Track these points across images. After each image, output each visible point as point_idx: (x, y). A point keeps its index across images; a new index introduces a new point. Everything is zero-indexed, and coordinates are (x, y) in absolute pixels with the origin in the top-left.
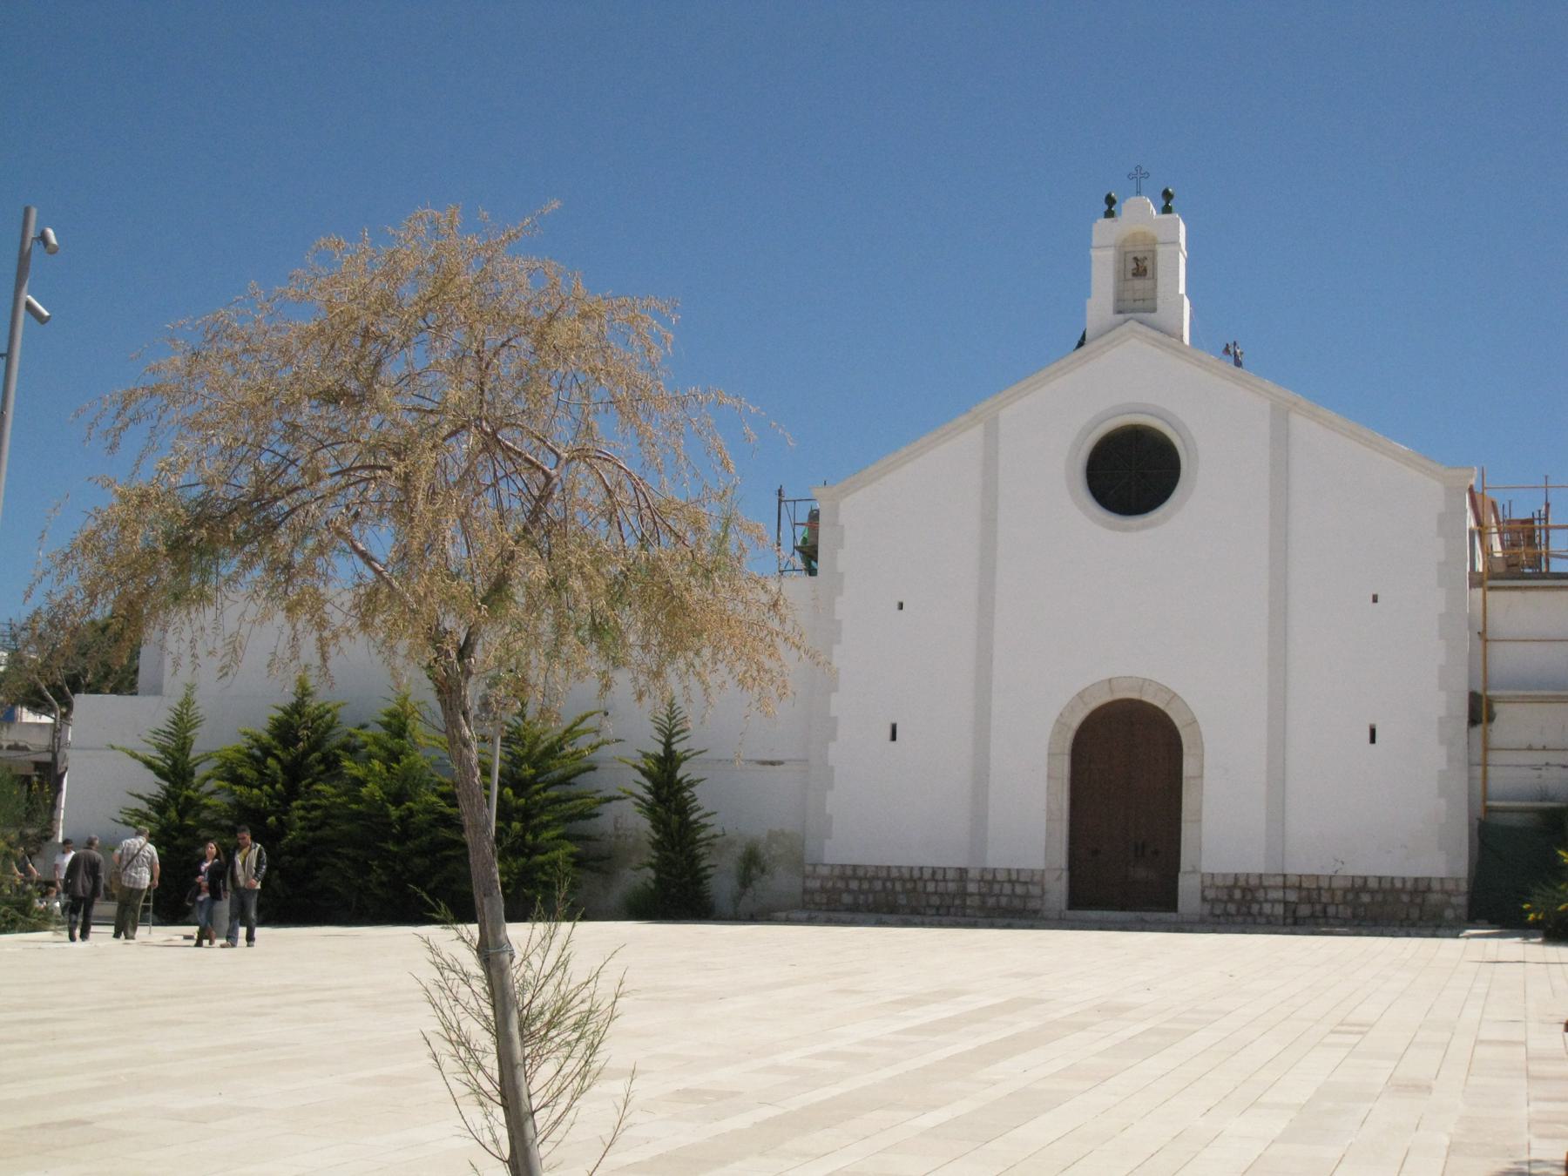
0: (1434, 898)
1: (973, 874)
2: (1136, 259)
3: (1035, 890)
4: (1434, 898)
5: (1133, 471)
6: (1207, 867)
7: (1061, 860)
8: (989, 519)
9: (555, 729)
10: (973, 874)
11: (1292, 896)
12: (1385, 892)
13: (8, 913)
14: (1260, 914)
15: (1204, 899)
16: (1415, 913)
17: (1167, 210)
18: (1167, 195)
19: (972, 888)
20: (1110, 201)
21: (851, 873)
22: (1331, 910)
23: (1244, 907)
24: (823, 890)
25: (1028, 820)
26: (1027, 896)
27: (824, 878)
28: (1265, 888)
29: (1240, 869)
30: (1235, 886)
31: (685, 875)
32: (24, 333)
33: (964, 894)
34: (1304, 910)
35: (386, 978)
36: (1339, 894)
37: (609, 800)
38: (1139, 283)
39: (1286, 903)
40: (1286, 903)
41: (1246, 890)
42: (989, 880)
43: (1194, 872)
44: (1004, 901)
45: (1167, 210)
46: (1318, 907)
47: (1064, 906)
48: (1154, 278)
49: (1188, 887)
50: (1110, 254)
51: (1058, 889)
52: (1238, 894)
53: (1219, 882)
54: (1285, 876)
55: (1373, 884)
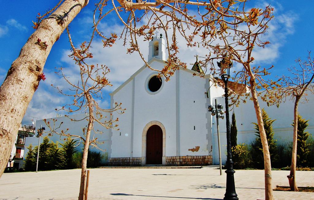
0: (206, 160)
1: (131, 158)
2: (157, 47)
3: (140, 161)
4: (206, 160)
6: (167, 155)
8: (133, 95)
9: (305, 121)
10: (131, 158)
11: (181, 160)
12: (197, 159)
14: (176, 164)
15: (166, 162)
16: (203, 163)
19: (131, 161)
21: (115, 159)
22: (188, 163)
23: (172, 163)
24: (110, 162)
25: (140, 151)
26: (139, 162)
27: (111, 160)
28: (176, 159)
29: (123, 157)
30: (194, 159)
31: (96, 161)
33: (130, 162)
34: (183, 163)
35: (67, 179)
36: (189, 160)
39: (180, 162)
40: (180, 162)
41: (173, 159)
43: (165, 157)
44: (136, 163)
46: (186, 162)
49: (164, 159)
51: (144, 160)
52: (172, 161)
53: (169, 158)
54: (180, 157)
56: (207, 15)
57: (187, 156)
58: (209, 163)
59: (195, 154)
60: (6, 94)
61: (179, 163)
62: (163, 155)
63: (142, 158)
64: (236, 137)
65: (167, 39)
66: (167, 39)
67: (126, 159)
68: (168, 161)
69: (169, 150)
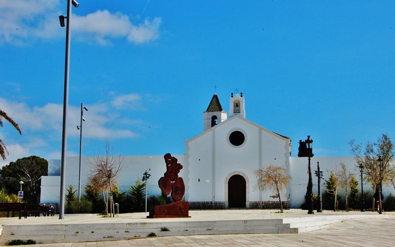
0: (285, 204)
4: (285, 204)
5: (237, 138)
7: (227, 200)
11: (264, 205)
13: (1, 217)
17: (242, 96)
18: (241, 94)
19: (213, 205)
20: (232, 94)
25: (222, 195)
32: (70, 77)
33: (212, 206)
34: (265, 207)
37: (319, 168)
38: (237, 108)
41: (257, 204)
42: (216, 203)
45: (242, 96)
47: (373, 196)
48: (240, 107)
49: (247, 204)
50: (233, 103)
51: (227, 204)
55: (276, 202)
56: (321, 183)
57: (269, 201)
58: (287, 207)
59: (277, 200)
60: (335, 190)
61: (262, 207)
62: (247, 200)
63: (226, 203)
64: (88, 13)
65: (318, 165)
66: (318, 165)
67: (207, 203)
68: (251, 205)
69: (252, 195)
